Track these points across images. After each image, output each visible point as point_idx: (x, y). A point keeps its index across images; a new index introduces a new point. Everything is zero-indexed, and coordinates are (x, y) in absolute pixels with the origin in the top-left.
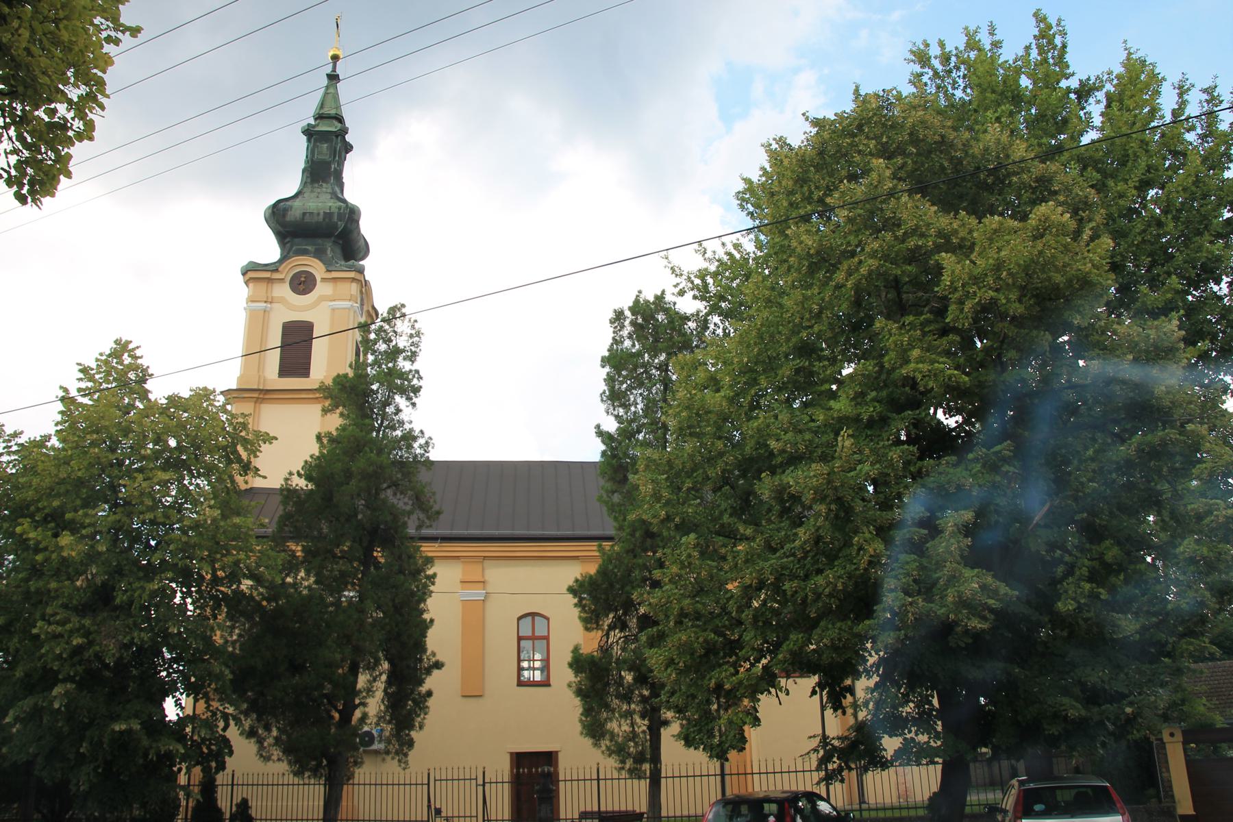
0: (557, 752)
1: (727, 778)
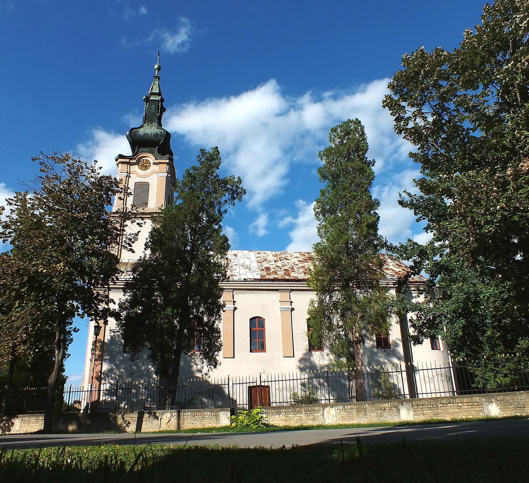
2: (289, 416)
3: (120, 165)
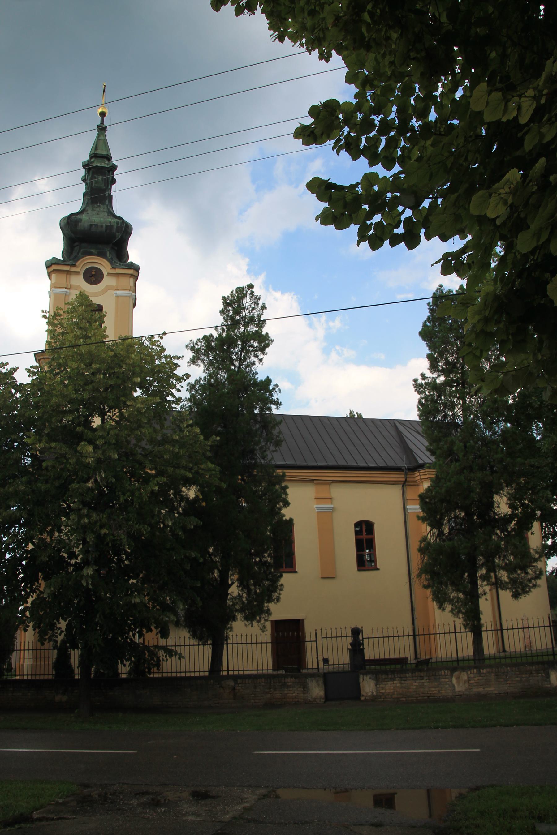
0: (303, 620)
1: (417, 637)
2: (405, 682)
3: (53, 276)
